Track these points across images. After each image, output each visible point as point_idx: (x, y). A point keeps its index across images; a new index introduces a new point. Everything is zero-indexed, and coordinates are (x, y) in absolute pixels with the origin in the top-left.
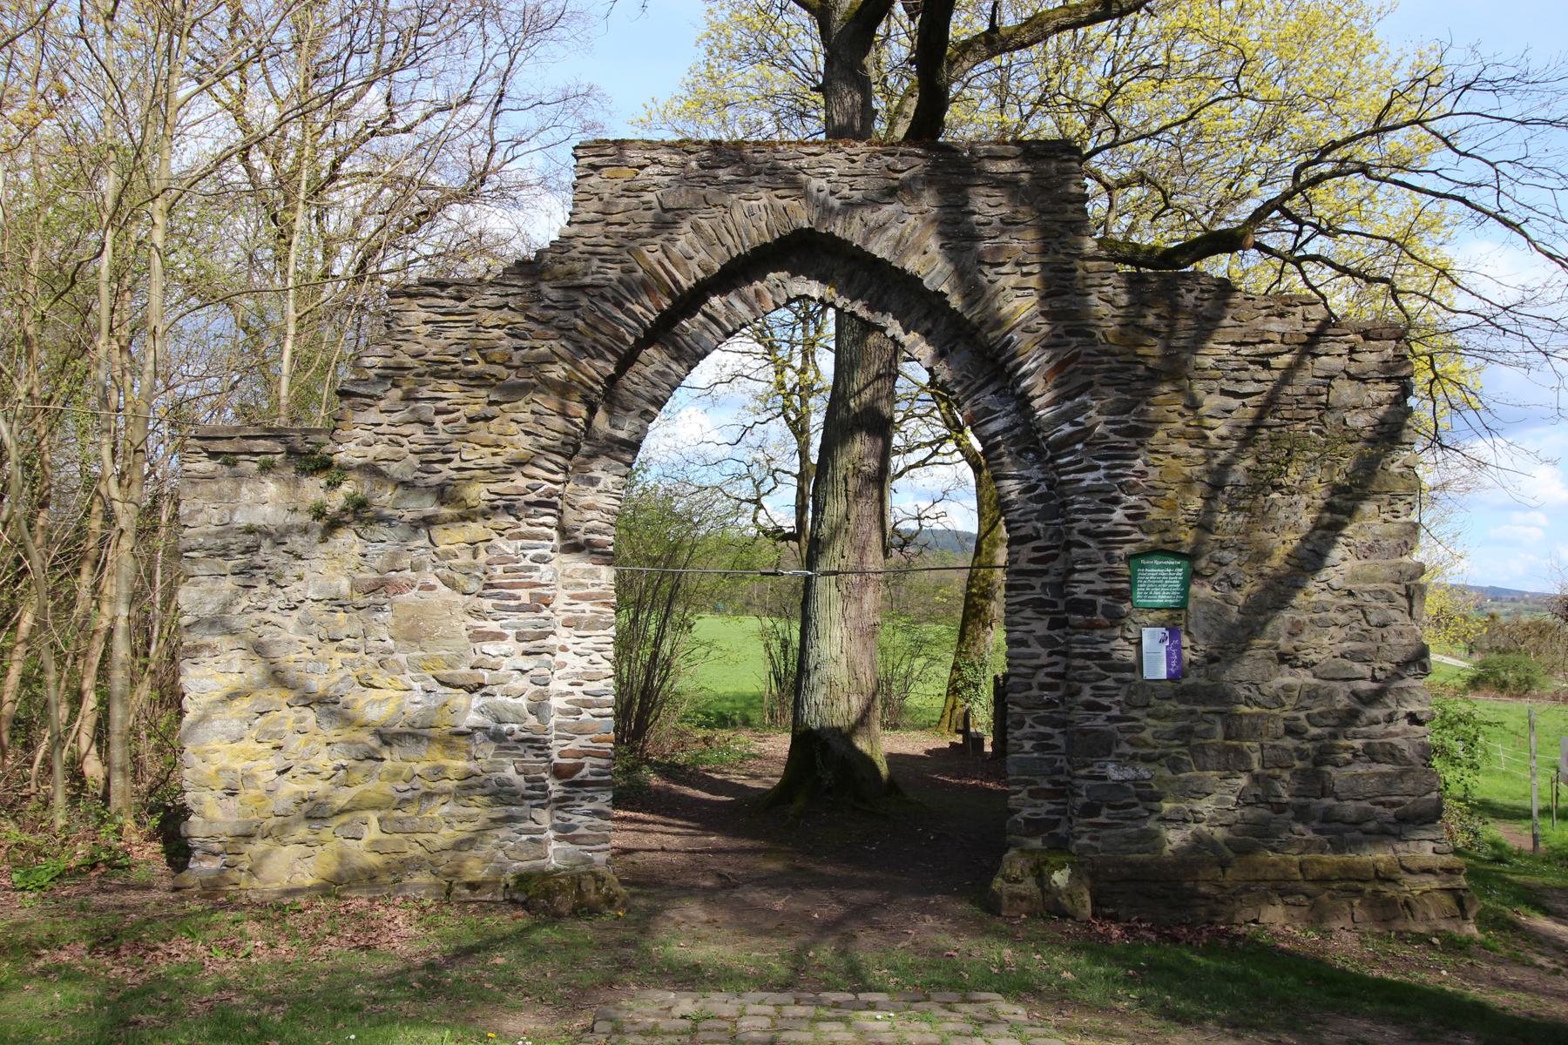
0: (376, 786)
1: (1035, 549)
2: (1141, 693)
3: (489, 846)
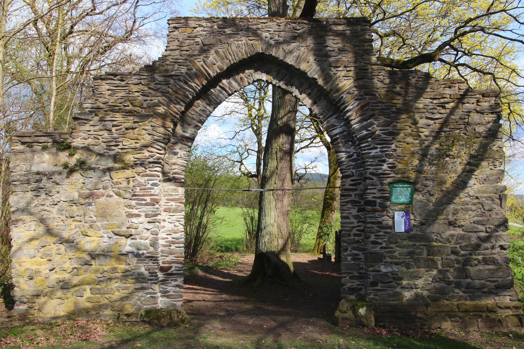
1: (352, 180)
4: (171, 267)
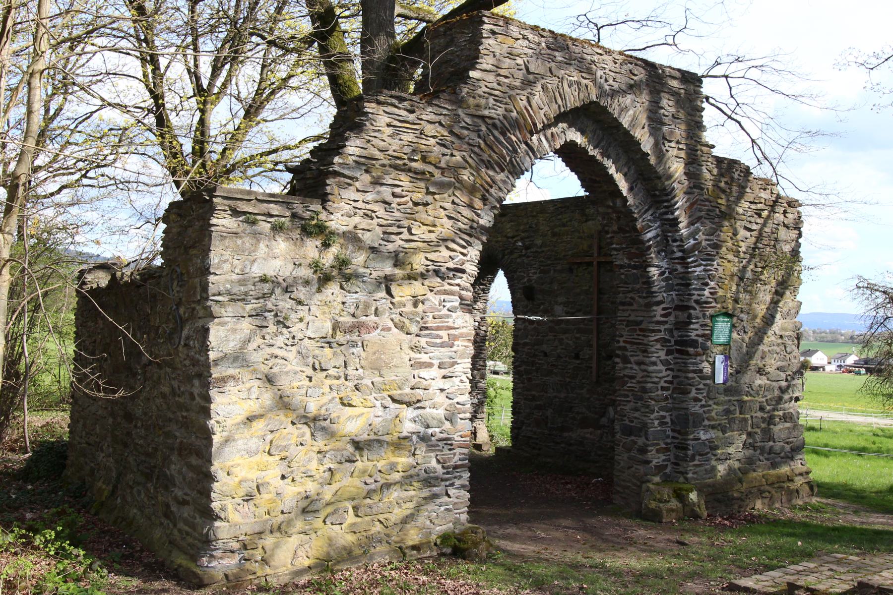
0: (348, 482)
1: (664, 309)
2: (712, 390)
3: (422, 520)
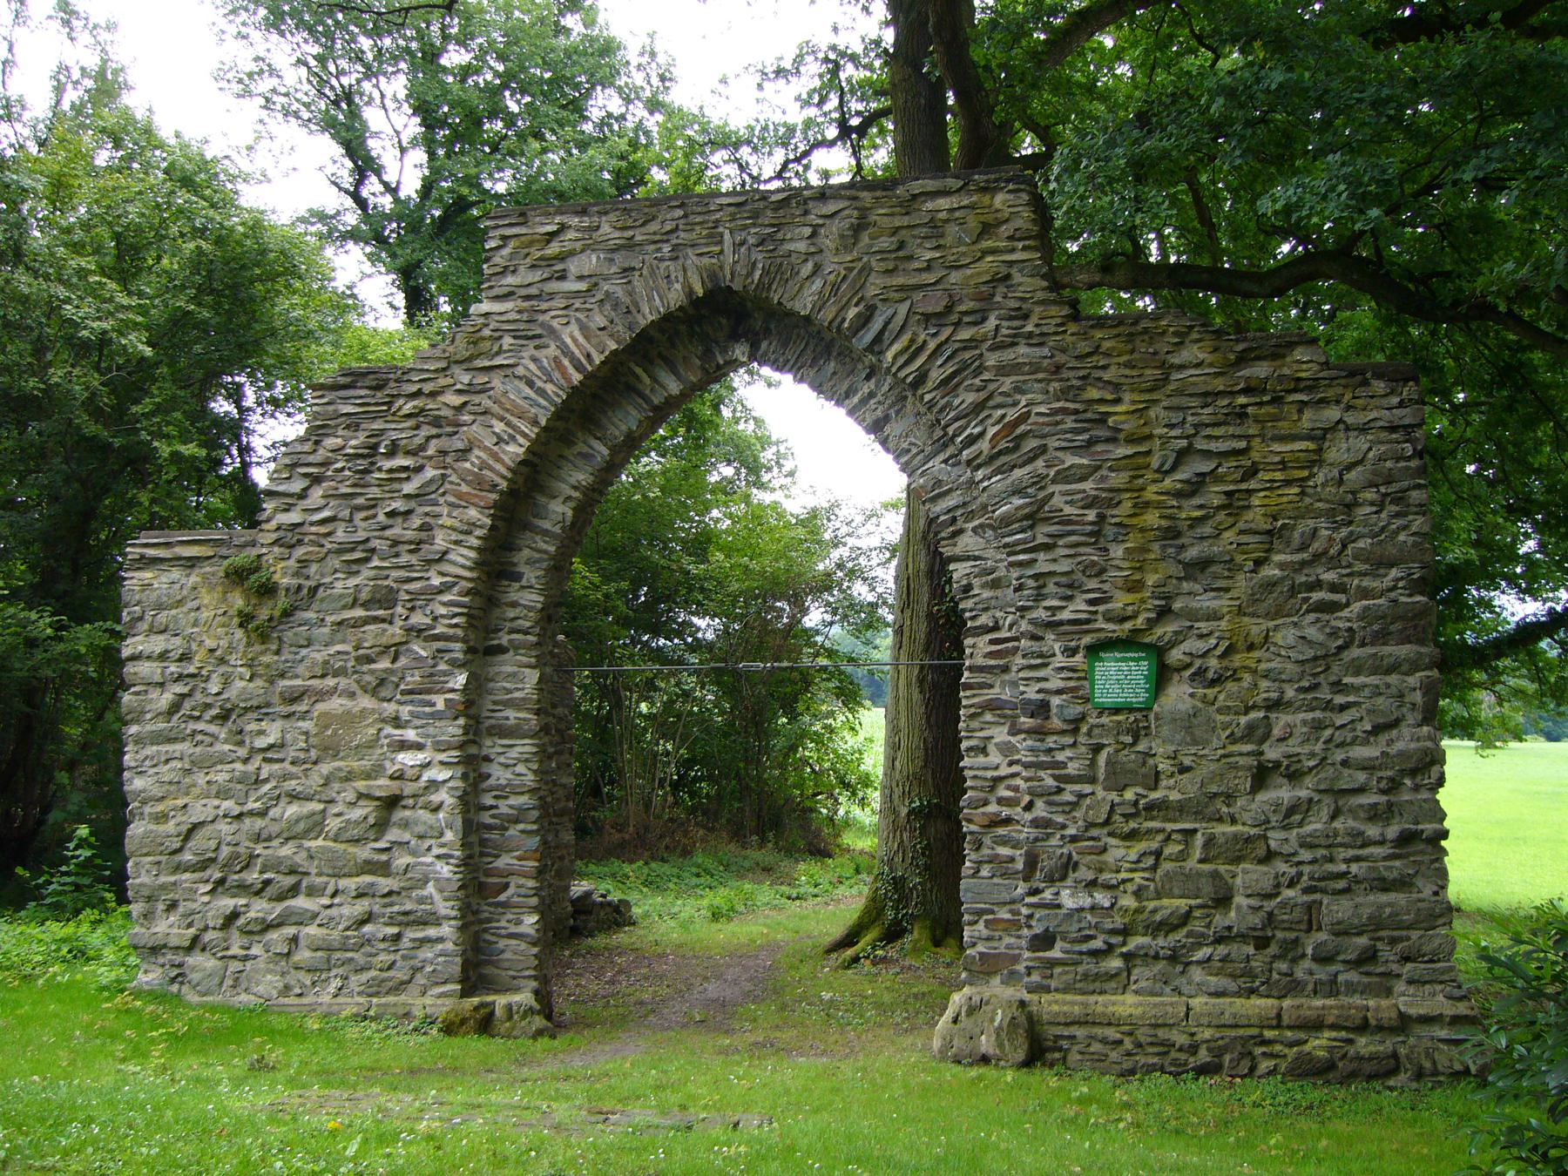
4: (506, 886)
